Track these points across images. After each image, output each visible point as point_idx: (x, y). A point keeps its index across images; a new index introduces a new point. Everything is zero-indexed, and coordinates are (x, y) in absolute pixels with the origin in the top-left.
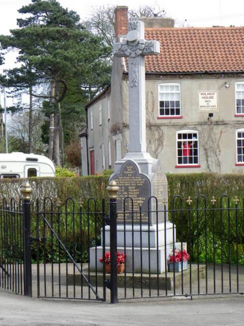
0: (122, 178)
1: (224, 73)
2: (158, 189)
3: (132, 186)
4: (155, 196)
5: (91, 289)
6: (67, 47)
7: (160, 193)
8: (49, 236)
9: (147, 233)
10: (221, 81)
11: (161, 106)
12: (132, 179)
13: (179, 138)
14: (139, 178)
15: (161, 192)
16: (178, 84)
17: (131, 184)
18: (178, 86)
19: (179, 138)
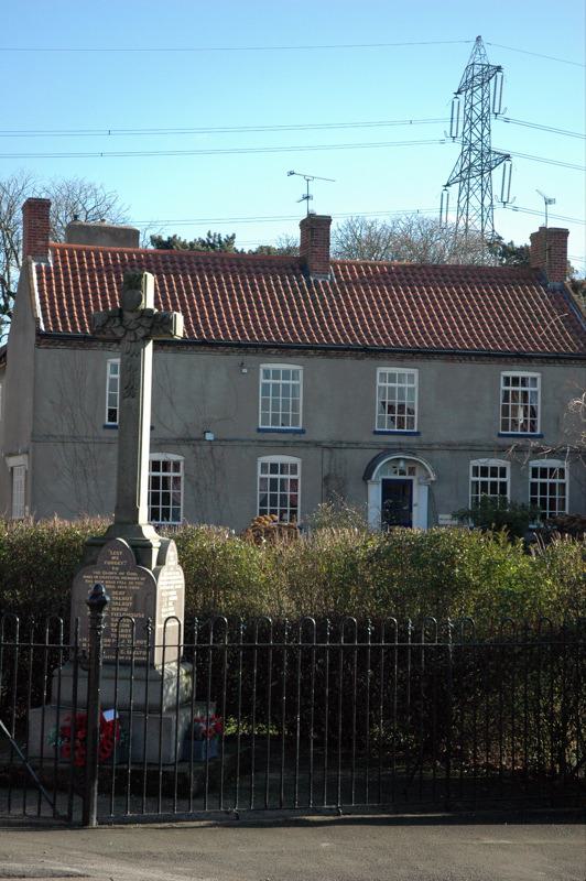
0: (99, 573)
1: (314, 348)
2: (168, 597)
3: (120, 590)
4: (167, 616)
5: (43, 798)
6: (503, 254)
7: (170, 604)
8: (171, 668)
9: (144, 683)
10: (235, 358)
11: (503, 415)
12: (120, 576)
13: (533, 477)
14: (135, 574)
15: (174, 602)
16: (415, 372)
17: (116, 585)
18: (413, 375)
19: (533, 477)
